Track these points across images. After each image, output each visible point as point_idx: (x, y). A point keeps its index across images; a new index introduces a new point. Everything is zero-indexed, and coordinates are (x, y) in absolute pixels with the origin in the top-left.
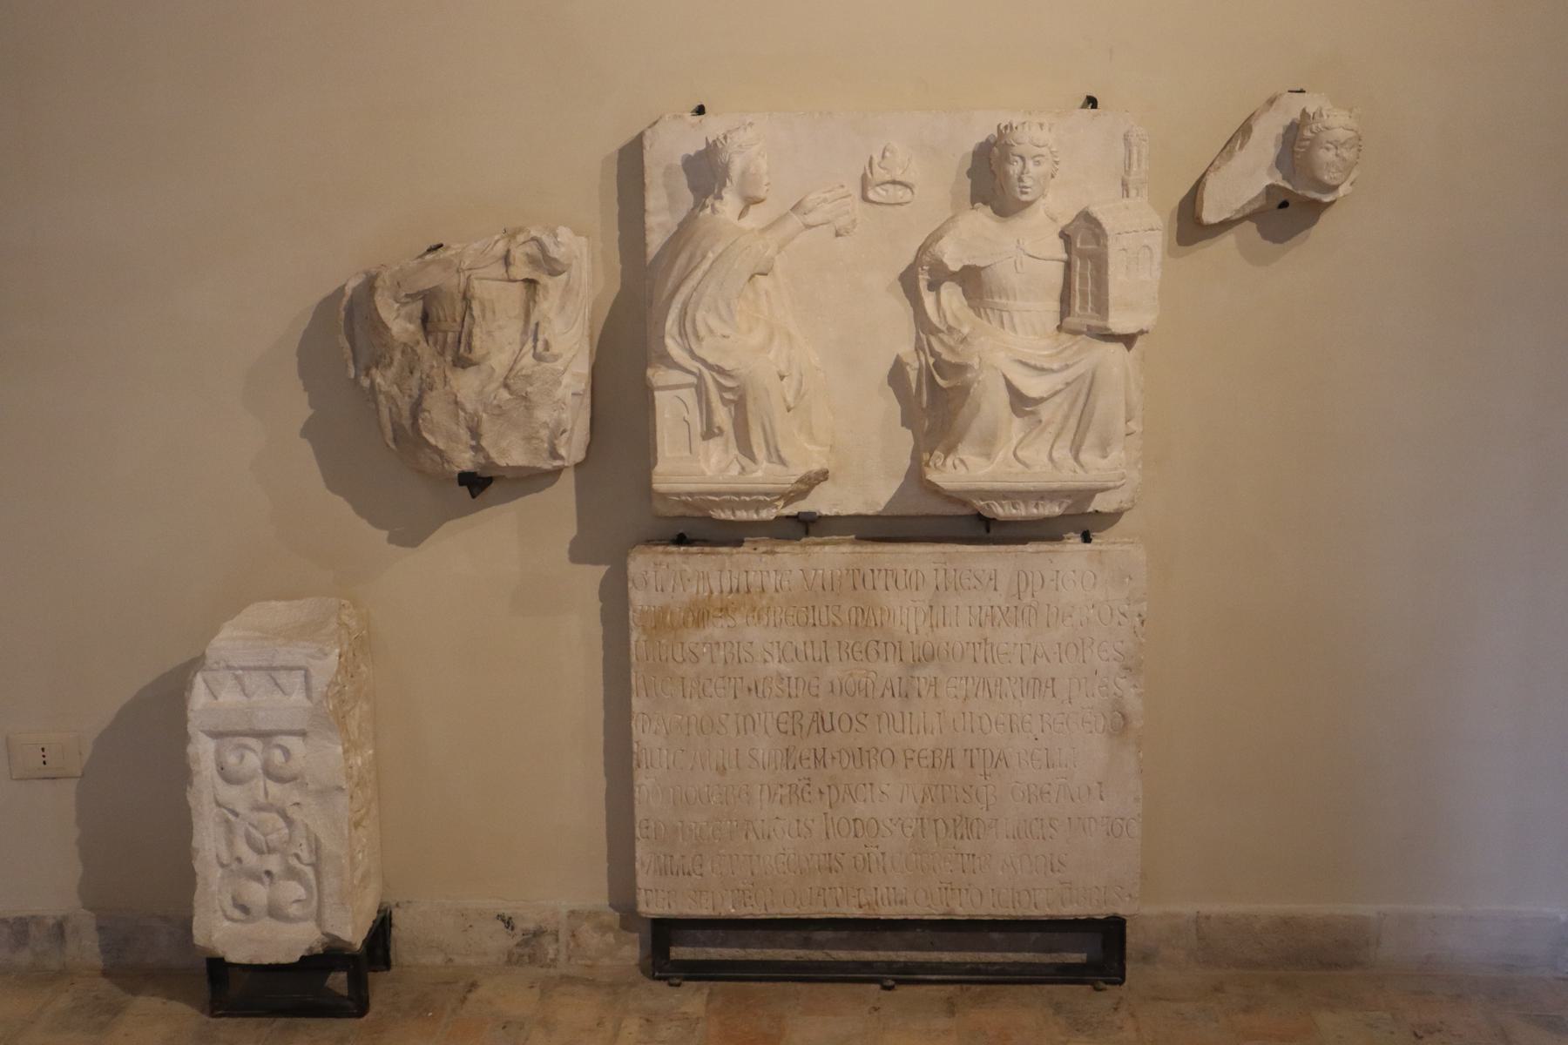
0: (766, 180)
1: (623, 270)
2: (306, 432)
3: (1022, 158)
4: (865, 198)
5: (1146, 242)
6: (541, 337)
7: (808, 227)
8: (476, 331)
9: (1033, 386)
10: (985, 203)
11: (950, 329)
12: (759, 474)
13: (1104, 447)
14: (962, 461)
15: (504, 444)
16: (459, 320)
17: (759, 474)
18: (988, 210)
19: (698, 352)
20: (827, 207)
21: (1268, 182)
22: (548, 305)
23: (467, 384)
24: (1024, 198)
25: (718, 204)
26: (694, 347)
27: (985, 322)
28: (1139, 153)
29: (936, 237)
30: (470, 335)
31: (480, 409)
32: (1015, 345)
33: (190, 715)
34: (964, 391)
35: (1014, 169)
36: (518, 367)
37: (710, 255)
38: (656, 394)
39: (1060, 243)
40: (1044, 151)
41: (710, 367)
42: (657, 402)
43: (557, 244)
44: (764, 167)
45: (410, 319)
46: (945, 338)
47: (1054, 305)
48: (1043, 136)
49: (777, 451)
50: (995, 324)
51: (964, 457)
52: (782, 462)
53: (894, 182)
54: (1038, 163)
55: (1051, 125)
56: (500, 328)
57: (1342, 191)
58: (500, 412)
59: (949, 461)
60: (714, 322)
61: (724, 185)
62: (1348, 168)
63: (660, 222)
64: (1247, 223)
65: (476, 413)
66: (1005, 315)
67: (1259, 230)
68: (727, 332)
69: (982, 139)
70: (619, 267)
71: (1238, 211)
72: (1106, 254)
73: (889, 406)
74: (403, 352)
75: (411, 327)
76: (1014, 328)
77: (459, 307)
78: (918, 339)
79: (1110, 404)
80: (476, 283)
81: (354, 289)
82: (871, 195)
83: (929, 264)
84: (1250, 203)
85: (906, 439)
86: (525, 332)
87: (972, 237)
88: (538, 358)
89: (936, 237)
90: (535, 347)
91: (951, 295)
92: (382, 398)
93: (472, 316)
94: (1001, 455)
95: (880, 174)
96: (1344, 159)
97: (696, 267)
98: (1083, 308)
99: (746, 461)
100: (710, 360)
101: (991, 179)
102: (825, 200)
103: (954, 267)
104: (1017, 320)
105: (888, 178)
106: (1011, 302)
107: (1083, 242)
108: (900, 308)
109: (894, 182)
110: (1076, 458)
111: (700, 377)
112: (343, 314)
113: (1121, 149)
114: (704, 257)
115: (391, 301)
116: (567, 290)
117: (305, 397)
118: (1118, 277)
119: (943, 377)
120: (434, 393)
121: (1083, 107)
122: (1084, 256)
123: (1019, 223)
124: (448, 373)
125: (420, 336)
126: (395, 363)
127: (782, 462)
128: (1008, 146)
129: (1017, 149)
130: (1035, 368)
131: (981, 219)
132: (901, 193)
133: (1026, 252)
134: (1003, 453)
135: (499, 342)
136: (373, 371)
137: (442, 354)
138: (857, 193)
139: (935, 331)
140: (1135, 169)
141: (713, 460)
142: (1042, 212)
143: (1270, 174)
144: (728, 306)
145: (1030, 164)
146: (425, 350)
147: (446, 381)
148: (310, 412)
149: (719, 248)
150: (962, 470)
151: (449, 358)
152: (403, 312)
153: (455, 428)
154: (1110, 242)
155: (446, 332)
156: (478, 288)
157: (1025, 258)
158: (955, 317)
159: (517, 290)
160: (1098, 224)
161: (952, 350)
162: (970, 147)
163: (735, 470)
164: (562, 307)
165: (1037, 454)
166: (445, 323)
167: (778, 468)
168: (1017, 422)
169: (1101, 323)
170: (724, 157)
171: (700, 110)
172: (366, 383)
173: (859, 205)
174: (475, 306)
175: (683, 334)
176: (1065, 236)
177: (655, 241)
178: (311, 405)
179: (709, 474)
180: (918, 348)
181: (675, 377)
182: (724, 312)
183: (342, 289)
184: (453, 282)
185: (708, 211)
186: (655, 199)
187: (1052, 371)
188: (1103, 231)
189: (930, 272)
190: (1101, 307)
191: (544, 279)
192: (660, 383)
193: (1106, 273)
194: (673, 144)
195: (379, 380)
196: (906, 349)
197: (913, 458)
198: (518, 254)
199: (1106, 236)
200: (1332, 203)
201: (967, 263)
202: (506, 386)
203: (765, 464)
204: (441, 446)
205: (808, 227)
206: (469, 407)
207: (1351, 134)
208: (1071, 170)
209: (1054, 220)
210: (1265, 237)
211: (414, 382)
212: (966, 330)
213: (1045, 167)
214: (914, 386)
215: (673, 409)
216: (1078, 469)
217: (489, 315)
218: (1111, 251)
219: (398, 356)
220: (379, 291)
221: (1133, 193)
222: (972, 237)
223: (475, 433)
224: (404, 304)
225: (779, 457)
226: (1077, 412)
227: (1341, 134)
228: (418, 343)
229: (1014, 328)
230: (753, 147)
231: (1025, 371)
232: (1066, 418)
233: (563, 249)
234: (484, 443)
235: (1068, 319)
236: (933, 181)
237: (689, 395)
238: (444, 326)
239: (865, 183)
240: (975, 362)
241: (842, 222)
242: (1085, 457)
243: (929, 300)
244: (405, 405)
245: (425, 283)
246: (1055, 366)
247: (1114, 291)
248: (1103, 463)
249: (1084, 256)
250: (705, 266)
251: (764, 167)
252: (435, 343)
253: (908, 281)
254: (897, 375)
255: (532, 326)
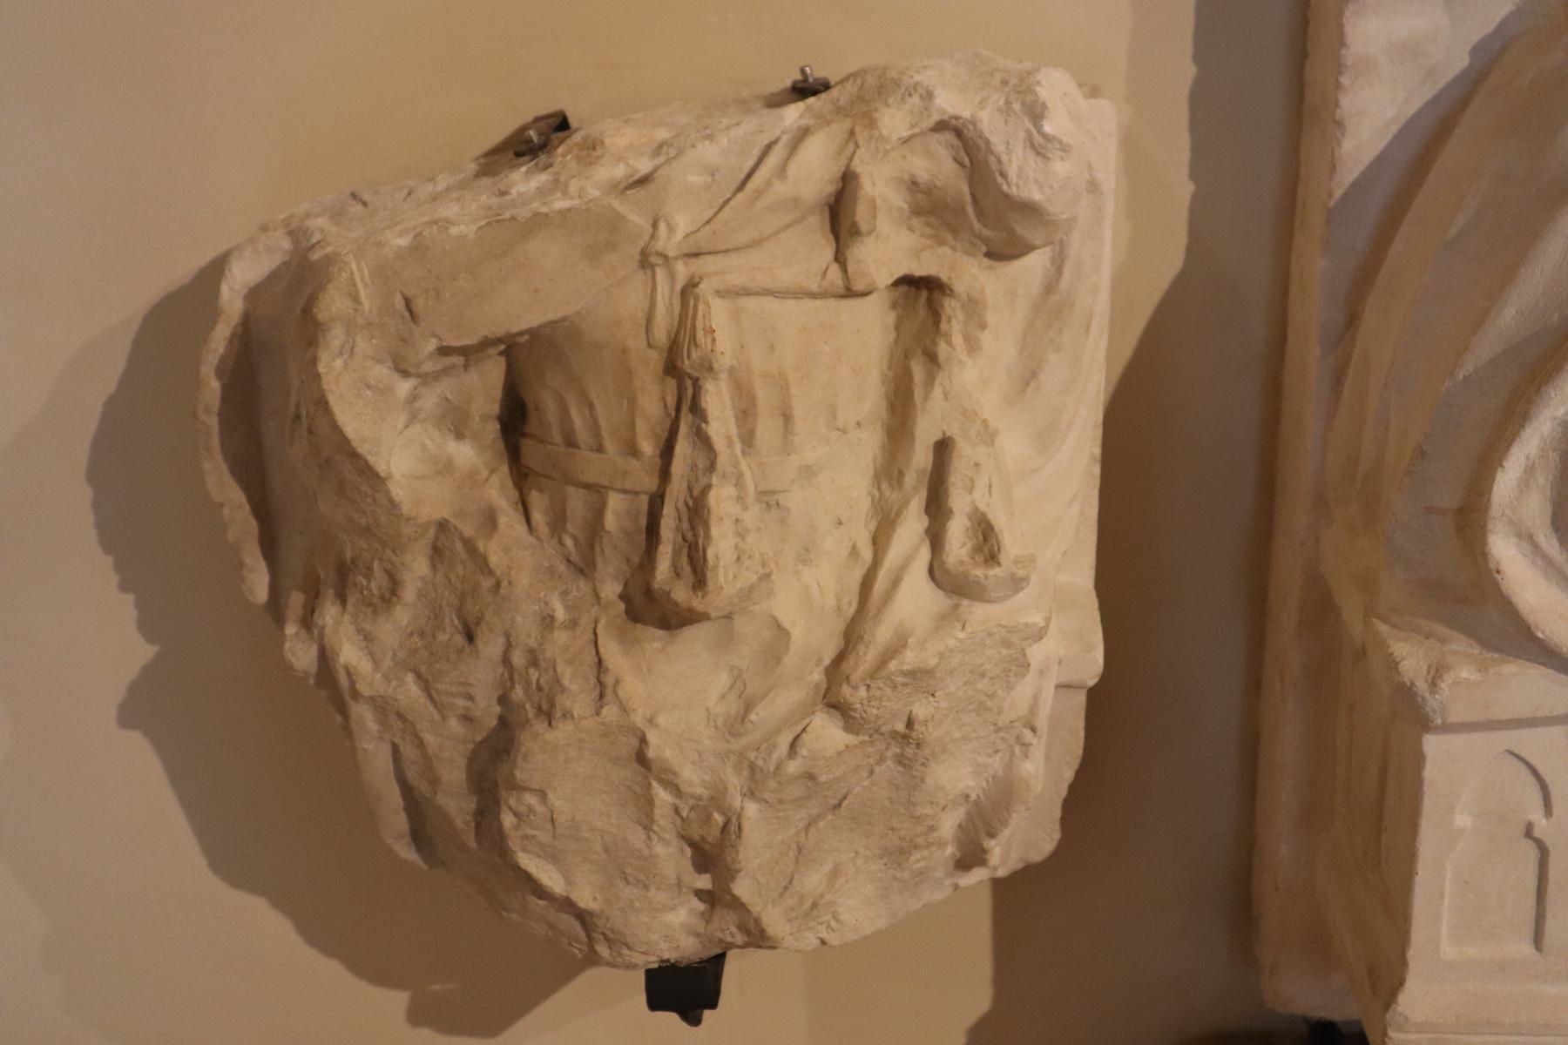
1: (1196, 199)
2: (141, 708)
6: (959, 502)
8: (721, 500)
15: (812, 881)
16: (648, 448)
22: (976, 378)
23: (678, 692)
30: (697, 512)
31: (735, 782)
36: (881, 634)
38: (1432, 744)
43: (1040, 146)
45: (456, 422)
56: (808, 472)
58: (823, 798)
65: (717, 798)
70: (1185, 189)
74: (437, 554)
75: (464, 453)
77: (652, 400)
80: (717, 315)
81: (254, 294)
86: (889, 471)
88: (953, 585)
90: (936, 538)
92: (363, 715)
93: (703, 440)
112: (213, 387)
115: (381, 372)
116: (1051, 306)
117: (126, 606)
120: (562, 732)
124: (611, 650)
125: (498, 491)
126: (409, 594)
135: (794, 526)
136: (329, 614)
137: (585, 567)
146: (518, 551)
147: (602, 690)
148: (146, 652)
151: (611, 589)
152: (430, 401)
153: (636, 837)
155: (597, 492)
156: (724, 331)
159: (869, 327)
164: (1028, 377)
166: (594, 442)
172: (302, 656)
174: (718, 401)
178: (147, 629)
183: (215, 270)
184: (625, 307)
191: (968, 273)
192: (1457, 714)
195: (350, 654)
198: (880, 186)
202: (836, 706)
204: (586, 898)
206: (692, 777)
211: (480, 673)
217: (767, 429)
219: (417, 568)
220: (336, 337)
223: (711, 855)
224: (426, 379)
228: (490, 520)
233: (1061, 168)
234: (742, 888)
238: (590, 467)
244: (449, 750)
245: (517, 311)
252: (558, 522)
255: (921, 456)
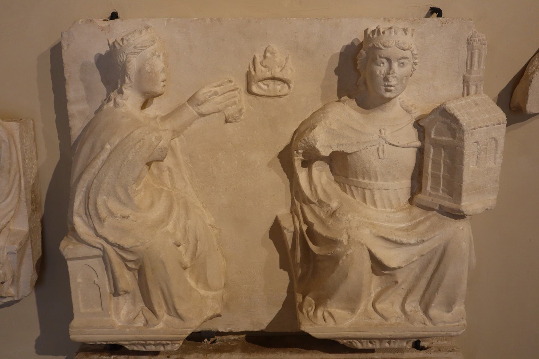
0: (162, 76)
3: (389, 60)
4: (249, 91)
5: (493, 134)
7: (202, 115)
9: (391, 257)
10: (350, 97)
11: (320, 202)
12: (161, 325)
13: (449, 305)
14: (330, 314)
17: (161, 325)
18: (354, 102)
19: (100, 231)
20: (218, 99)
24: (388, 95)
25: (118, 100)
26: (97, 227)
27: (349, 197)
28: (480, 56)
29: (308, 125)
32: (377, 222)
34: (334, 260)
35: (381, 69)
37: (108, 147)
38: (69, 263)
39: (413, 133)
40: (408, 54)
41: (112, 244)
42: (70, 269)
44: (159, 64)
46: (317, 209)
47: (406, 183)
48: (408, 40)
49: (175, 309)
50: (359, 199)
51: (332, 310)
52: (179, 316)
53: (274, 79)
54: (402, 65)
55: (413, 30)
59: (320, 313)
60: (114, 205)
61: (124, 82)
63: (79, 111)
66: (367, 193)
68: (127, 212)
69: (348, 42)
72: (462, 147)
73: (269, 254)
76: (375, 204)
78: (293, 203)
79: (458, 271)
82: (255, 89)
83: (303, 148)
85: (283, 279)
87: (340, 126)
89: (308, 125)
91: (321, 174)
94: (362, 307)
95: (262, 71)
97: (96, 158)
98: (435, 188)
99: (149, 315)
100: (111, 239)
101: (357, 75)
102: (216, 93)
103: (325, 152)
104: (377, 196)
105: (268, 75)
106: (373, 182)
107: (436, 134)
108: (277, 179)
109: (274, 79)
110: (426, 311)
111: (104, 251)
113: (464, 52)
114: (102, 148)
118: (470, 166)
119: (315, 243)
121: (428, 16)
122: (437, 145)
123: (380, 116)
127: (179, 316)
128: (375, 48)
129: (385, 52)
130: (395, 242)
131: (346, 112)
132: (279, 87)
133: (385, 138)
134: (365, 304)
138: (242, 87)
139: (306, 201)
140: (475, 68)
141: (124, 311)
142: (398, 105)
144: (126, 190)
145: (395, 65)
149: (116, 140)
150: (330, 323)
154: (466, 137)
157: (387, 147)
158: (325, 191)
160: (455, 120)
161: (322, 222)
162: (338, 49)
163: (140, 323)
165: (391, 306)
167: (177, 321)
168: (376, 280)
169: (454, 206)
170: (122, 57)
171: (114, 16)
173: (243, 96)
175: (87, 214)
176: (420, 126)
177: (77, 126)
179: (118, 324)
180: (293, 212)
181: (83, 250)
182: (123, 197)
185: (111, 104)
186: (74, 91)
187: (410, 244)
188: (460, 126)
189: (304, 154)
190: (454, 188)
192: (70, 256)
193: (461, 163)
194: (86, 45)
196: (283, 212)
197: (288, 292)
199: (463, 131)
201: (336, 149)
203: (166, 316)
205: (202, 115)
208: (427, 72)
209: (408, 112)
212: (334, 205)
213: (408, 68)
214: (290, 244)
215: (83, 274)
216: (428, 323)
218: (466, 144)
221: (473, 89)
222: (340, 126)
225: (177, 313)
226: (428, 274)
229: (375, 204)
230: (147, 44)
231: (388, 245)
232: (418, 279)
235: (420, 196)
236: (305, 80)
237: (97, 264)
239: (249, 79)
240: (344, 239)
241: (231, 111)
242: (434, 312)
243: (302, 175)
246: (413, 241)
247: (467, 178)
248: (448, 316)
249: (437, 145)
250: (104, 156)
251: (159, 64)
253: (285, 159)
254: (276, 232)
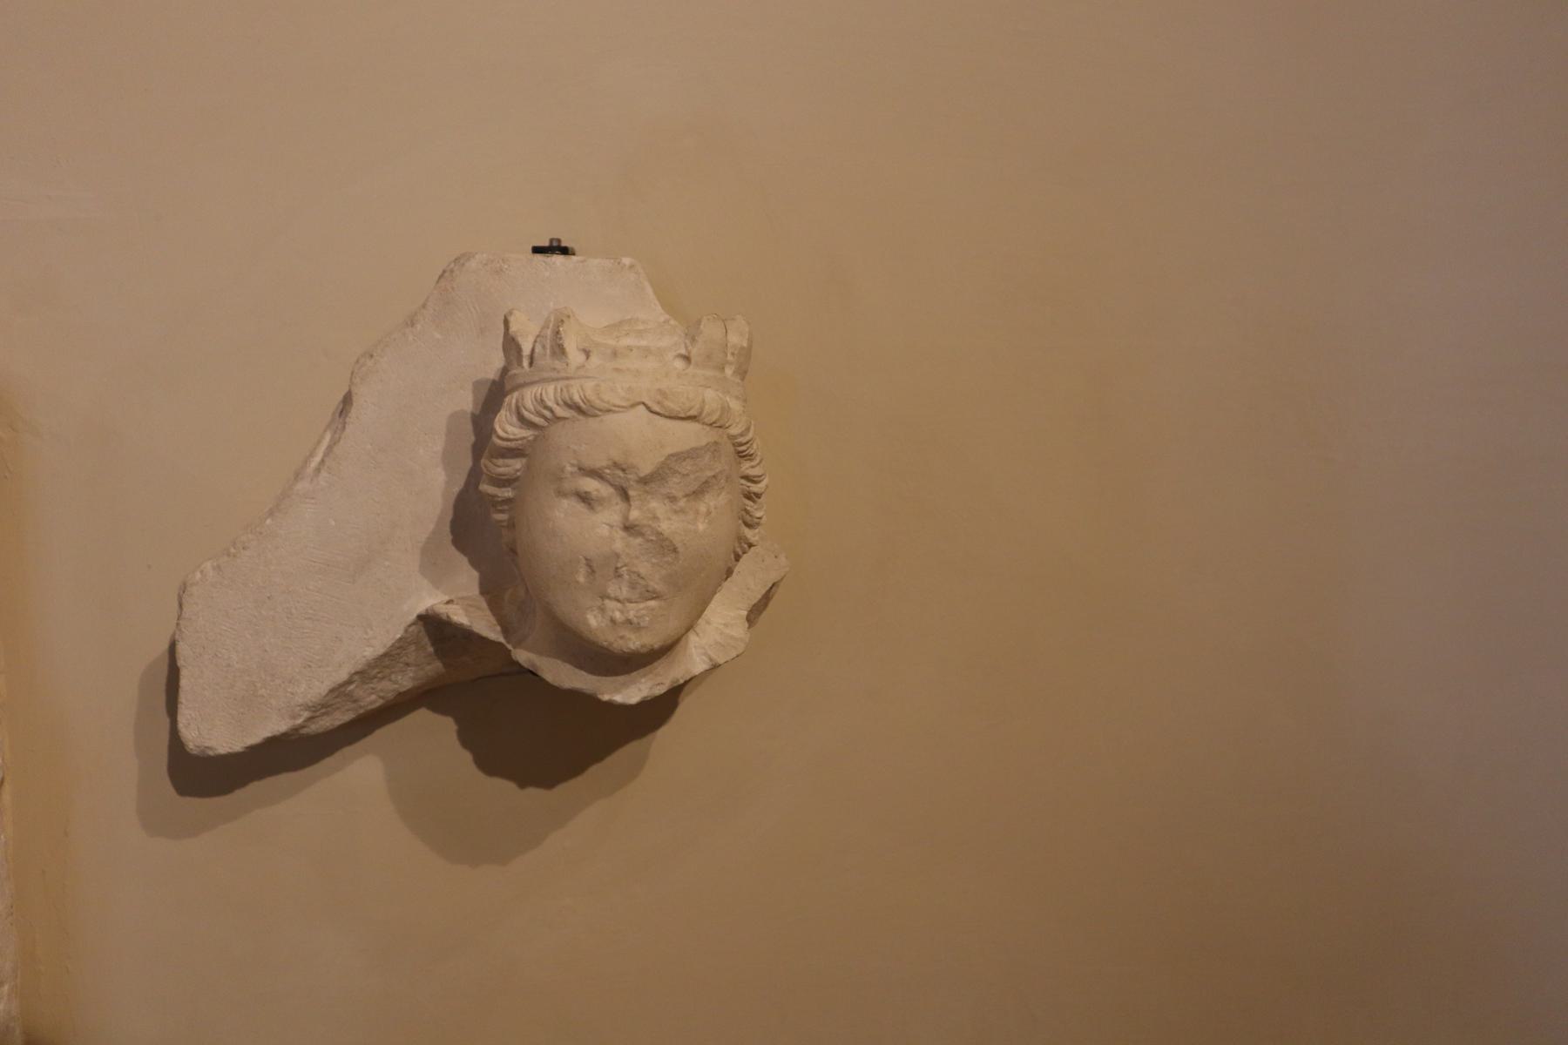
21: (430, 599)
33: (425, 582)
57: (694, 658)
62: (697, 585)
64: (422, 716)
67: (467, 738)
71: (321, 708)
84: (363, 675)
96: (664, 546)
143: (431, 567)
200: (660, 709)
207: (687, 436)
210: (489, 763)
227: (639, 437)
